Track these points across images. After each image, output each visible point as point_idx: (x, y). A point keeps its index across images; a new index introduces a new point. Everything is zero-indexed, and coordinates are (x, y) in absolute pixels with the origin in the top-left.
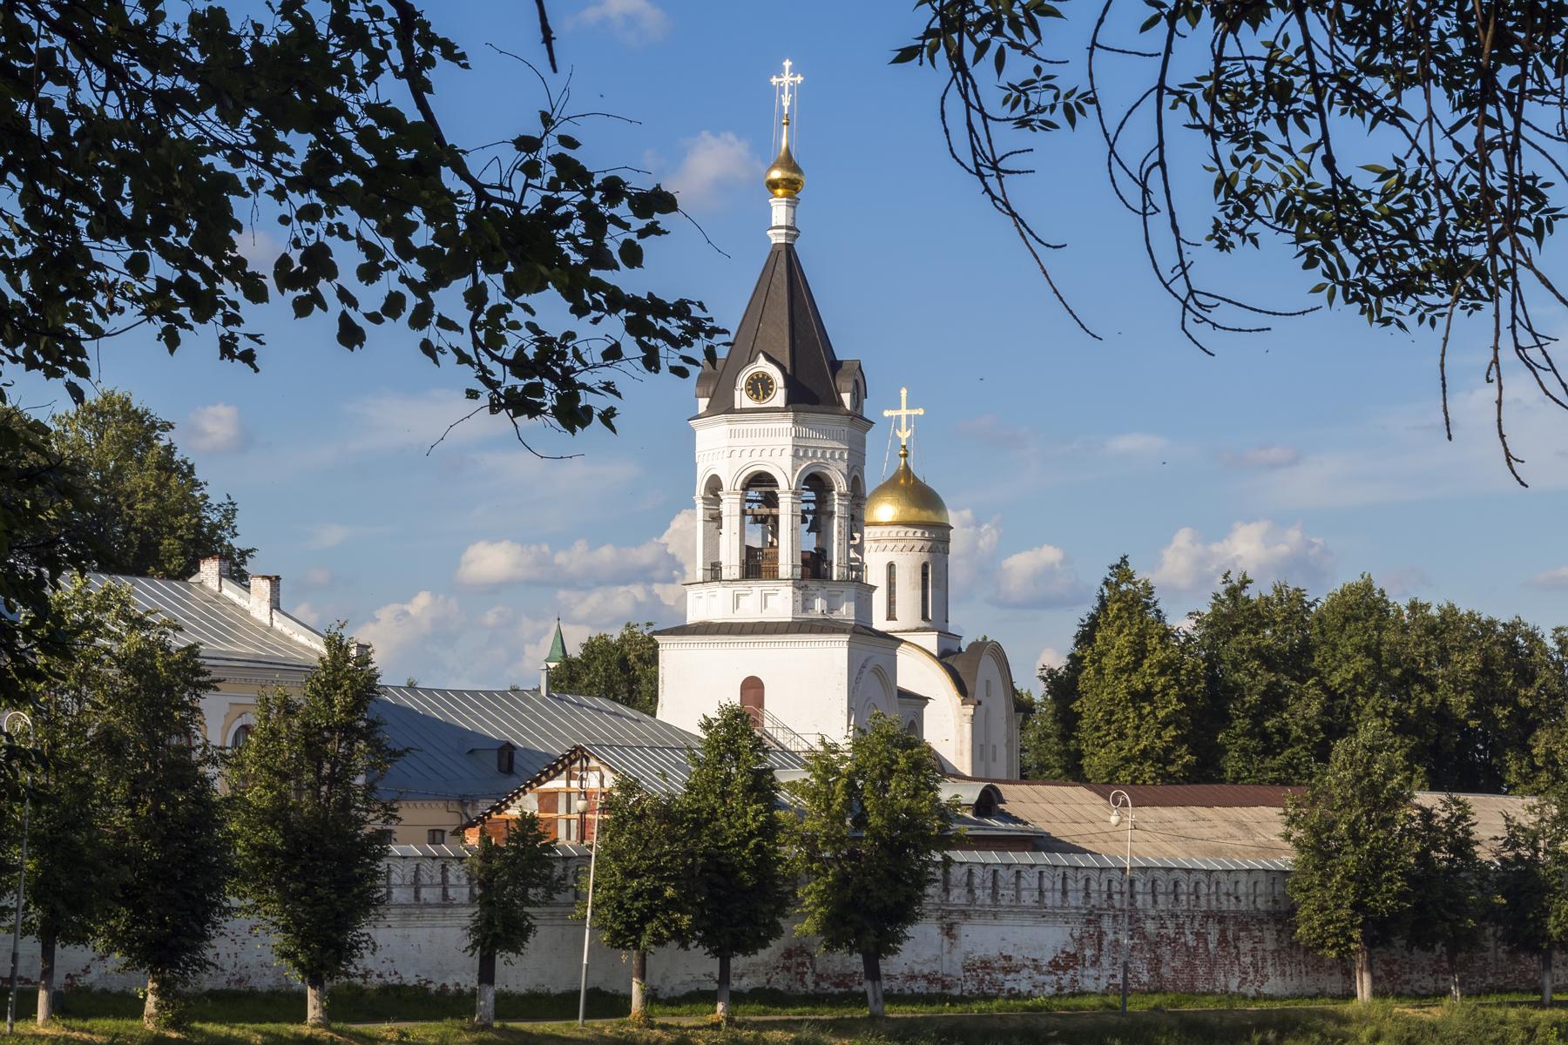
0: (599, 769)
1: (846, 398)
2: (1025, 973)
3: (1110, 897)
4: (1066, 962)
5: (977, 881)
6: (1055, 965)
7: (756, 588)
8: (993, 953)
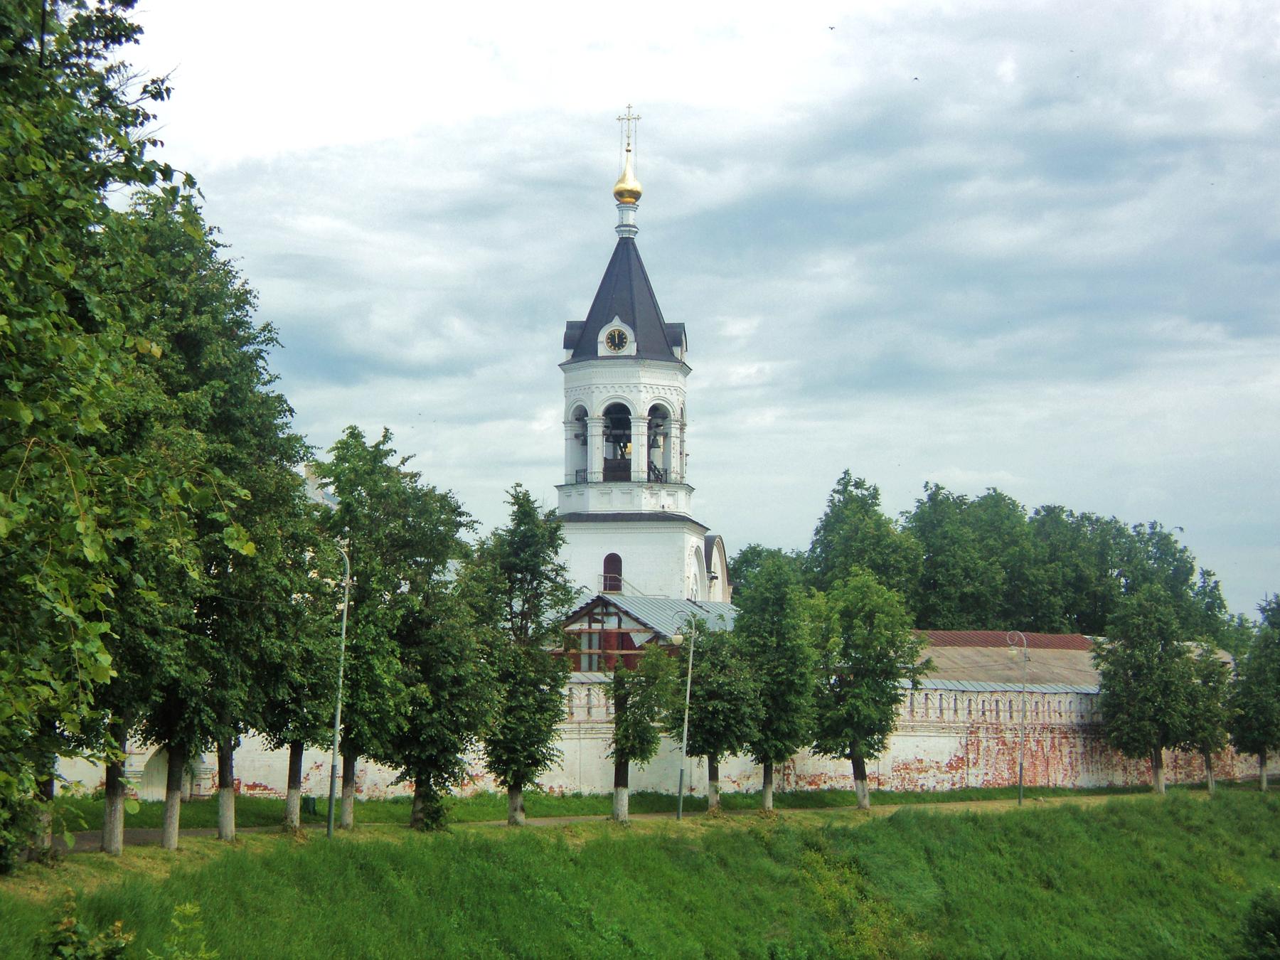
0: (616, 614)
1: (677, 351)
2: (931, 772)
3: (984, 713)
4: (958, 763)
6: (950, 766)
7: (617, 489)
8: (911, 757)
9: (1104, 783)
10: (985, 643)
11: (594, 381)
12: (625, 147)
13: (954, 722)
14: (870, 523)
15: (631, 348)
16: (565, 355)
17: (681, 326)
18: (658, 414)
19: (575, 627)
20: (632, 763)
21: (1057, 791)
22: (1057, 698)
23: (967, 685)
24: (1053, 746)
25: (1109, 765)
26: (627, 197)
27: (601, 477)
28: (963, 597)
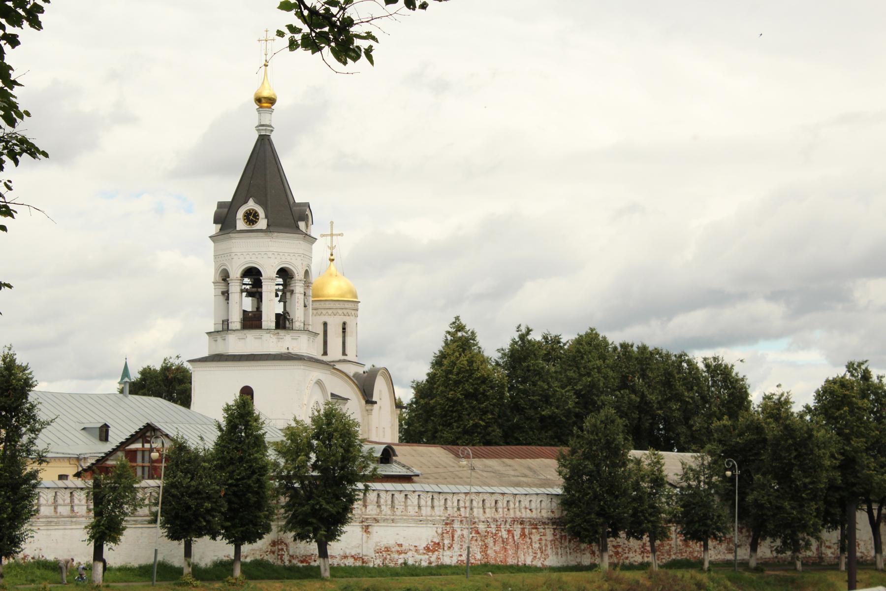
1: (302, 225)
2: (410, 554)
3: (459, 509)
5: (382, 501)
6: (427, 549)
7: (251, 335)
9: (574, 563)
10: (512, 456)
11: (234, 250)
12: (264, 62)
13: (431, 516)
14: (464, 360)
15: (262, 224)
16: (214, 229)
17: (307, 205)
18: (284, 273)
19: (133, 446)
20: (106, 548)
21: (526, 569)
22: (528, 498)
23: (445, 488)
24: (523, 535)
25: (577, 550)
26: (265, 102)
27: (273, 325)
28: (543, 419)
